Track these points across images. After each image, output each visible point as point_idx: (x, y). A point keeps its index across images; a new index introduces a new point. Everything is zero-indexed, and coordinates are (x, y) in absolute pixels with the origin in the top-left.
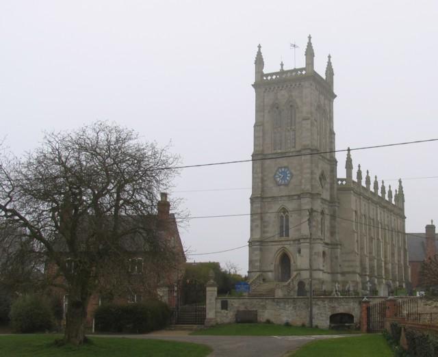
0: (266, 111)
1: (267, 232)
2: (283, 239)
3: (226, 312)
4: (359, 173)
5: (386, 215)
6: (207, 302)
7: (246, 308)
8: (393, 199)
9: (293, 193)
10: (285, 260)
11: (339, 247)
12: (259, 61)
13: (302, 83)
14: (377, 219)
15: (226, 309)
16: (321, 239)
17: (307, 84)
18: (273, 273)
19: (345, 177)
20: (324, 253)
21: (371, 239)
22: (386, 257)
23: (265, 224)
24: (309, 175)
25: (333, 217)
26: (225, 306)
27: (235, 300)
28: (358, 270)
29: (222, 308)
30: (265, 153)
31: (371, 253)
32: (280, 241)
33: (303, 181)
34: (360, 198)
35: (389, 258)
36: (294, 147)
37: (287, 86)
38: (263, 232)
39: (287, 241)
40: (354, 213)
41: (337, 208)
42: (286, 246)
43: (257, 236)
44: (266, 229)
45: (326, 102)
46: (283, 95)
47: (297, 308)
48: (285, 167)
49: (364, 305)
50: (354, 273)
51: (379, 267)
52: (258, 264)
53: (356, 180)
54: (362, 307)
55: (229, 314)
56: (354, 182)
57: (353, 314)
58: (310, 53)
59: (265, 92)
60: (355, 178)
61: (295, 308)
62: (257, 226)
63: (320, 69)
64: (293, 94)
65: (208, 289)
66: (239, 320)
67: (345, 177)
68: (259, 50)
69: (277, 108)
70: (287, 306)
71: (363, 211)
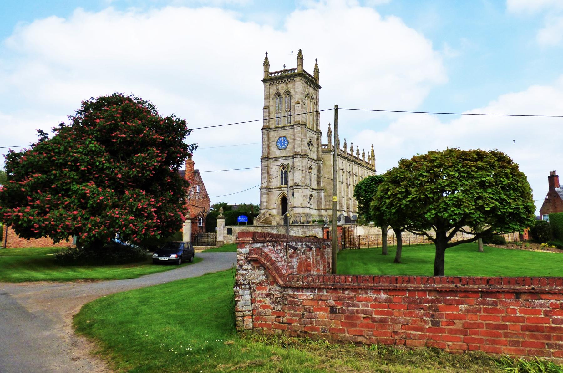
2: (283, 186)
3: (231, 236)
9: (288, 155)
12: (266, 64)
16: (308, 186)
17: (298, 79)
23: (271, 176)
26: (230, 232)
27: (237, 228)
30: (271, 127)
32: (281, 188)
36: (290, 123)
37: (285, 81)
38: (269, 181)
41: (321, 164)
42: (284, 191)
43: (265, 185)
46: (282, 87)
48: (283, 137)
49: (325, 230)
54: (323, 231)
58: (300, 57)
64: (289, 86)
65: (218, 220)
69: (279, 96)
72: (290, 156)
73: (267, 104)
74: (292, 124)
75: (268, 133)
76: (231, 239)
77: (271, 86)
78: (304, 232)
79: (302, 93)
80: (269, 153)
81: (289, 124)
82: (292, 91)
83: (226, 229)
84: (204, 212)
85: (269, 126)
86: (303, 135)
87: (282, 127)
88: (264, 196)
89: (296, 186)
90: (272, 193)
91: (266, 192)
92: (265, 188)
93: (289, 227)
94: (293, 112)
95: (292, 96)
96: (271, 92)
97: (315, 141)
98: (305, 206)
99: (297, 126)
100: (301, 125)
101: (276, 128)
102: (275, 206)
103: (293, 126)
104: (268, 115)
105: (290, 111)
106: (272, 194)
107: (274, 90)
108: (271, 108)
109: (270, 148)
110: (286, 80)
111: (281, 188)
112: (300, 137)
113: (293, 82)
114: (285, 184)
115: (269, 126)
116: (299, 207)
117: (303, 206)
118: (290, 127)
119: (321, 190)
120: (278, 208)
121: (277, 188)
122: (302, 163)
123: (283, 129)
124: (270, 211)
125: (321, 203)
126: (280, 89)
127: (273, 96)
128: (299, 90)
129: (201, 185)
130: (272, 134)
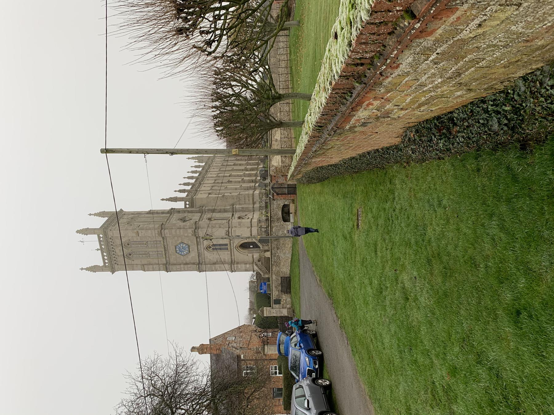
0: (133, 263)
2: (229, 247)
4: (181, 191)
5: (206, 182)
8: (201, 164)
10: (244, 246)
11: (235, 206)
12: (94, 269)
13: (110, 237)
14: (215, 177)
15: (280, 300)
16: (229, 221)
18: (254, 254)
19: (183, 202)
20: (239, 218)
21: (229, 182)
22: (243, 170)
24: (182, 230)
25: (213, 211)
26: (278, 302)
27: (274, 294)
28: (251, 192)
30: (165, 262)
31: (239, 182)
32: (231, 250)
33: (186, 235)
34: (206, 177)
35: (243, 168)
37: (112, 248)
39: (230, 244)
40: (210, 196)
41: (207, 208)
45: (125, 217)
50: (253, 195)
51: (250, 175)
52: (248, 266)
53: (186, 193)
56: (187, 196)
57: (282, 205)
58: (86, 231)
60: (184, 195)
62: (220, 267)
63: (100, 222)
65: (265, 315)
67: (183, 202)
68: (84, 269)
69: (130, 255)
71: (215, 176)
72: (197, 241)
74: (162, 239)
77: (119, 264)
80: (194, 264)
84: (256, 331)
87: (165, 250)
91: (235, 265)
97: (181, 215)
100: (162, 229)
102: (250, 255)
104: (151, 266)
108: (143, 263)
111: (231, 250)
114: (226, 245)
119: (233, 208)
127: (130, 261)
129: (226, 336)
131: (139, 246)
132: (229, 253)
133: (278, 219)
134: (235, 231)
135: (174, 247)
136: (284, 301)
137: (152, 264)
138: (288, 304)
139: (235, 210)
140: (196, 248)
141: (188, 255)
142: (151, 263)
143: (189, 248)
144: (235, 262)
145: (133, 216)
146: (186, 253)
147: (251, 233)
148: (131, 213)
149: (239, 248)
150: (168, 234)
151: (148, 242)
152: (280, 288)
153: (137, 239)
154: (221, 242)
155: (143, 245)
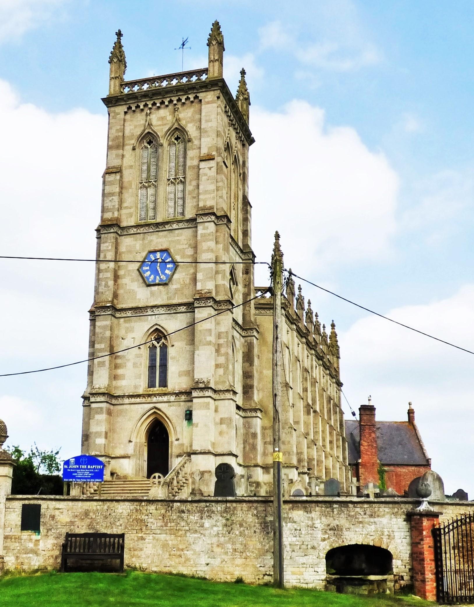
1: (122, 377)
2: (157, 389)
3: (35, 537)
6: (66, 574)
7: (90, 526)
13: (201, 95)
23: (119, 361)
29: (25, 526)
30: (124, 224)
37: (171, 101)
39: (165, 394)
42: (158, 406)
44: (120, 372)
45: (239, 146)
47: (236, 527)
48: (161, 251)
55: (41, 545)
57: (391, 549)
59: (126, 113)
61: (229, 526)
66: (70, 562)
69: (150, 143)
70: (207, 523)
72: (180, 305)
73: (116, 162)
74: (189, 215)
75: (116, 239)
76: (35, 552)
77: (128, 117)
78: (336, 530)
79: (218, 135)
80: (115, 296)
81: (180, 217)
82: (191, 130)
83: (18, 506)
85: (118, 219)
86: (221, 246)
87: (157, 225)
88: (98, 417)
89: (202, 389)
90: (121, 411)
91: (104, 405)
92: (103, 394)
93: (285, 507)
94: (194, 183)
95: (190, 141)
96: (127, 132)
98: (225, 451)
99: (206, 219)
100: (217, 217)
101: (137, 226)
102: (130, 449)
103: (193, 220)
104: (117, 190)
105: (183, 183)
106: (121, 412)
107: (136, 127)
108: (126, 173)
109: (120, 281)
110: (175, 99)
111: (149, 396)
112: (212, 251)
113: (196, 105)
114: (164, 383)
115: (118, 219)
116: (209, 453)
117: (219, 451)
118: (181, 225)
119: (255, 410)
120: (137, 455)
121: (139, 396)
122: (218, 323)
123: (161, 228)
124: (114, 465)
125: (254, 447)
126: (154, 122)
127: (133, 142)
128: (213, 124)
130: (126, 242)
131: (173, 164)
132: (141, 391)
133: (336, 530)
134: (207, 406)
135: (164, 247)
136: (31, 545)
137: (121, 193)
138: (17, 558)
139: (249, 414)
140: (159, 302)
141: (141, 280)
142: (124, 191)
143: (159, 285)
144: (112, 407)
145: (241, 162)
146: (148, 278)
147: (201, 453)
148: (246, 160)
149: (151, 418)
150: (204, 232)
151: (180, 187)
152: (83, 530)
153: (192, 159)
154: (173, 369)
155: (173, 173)
